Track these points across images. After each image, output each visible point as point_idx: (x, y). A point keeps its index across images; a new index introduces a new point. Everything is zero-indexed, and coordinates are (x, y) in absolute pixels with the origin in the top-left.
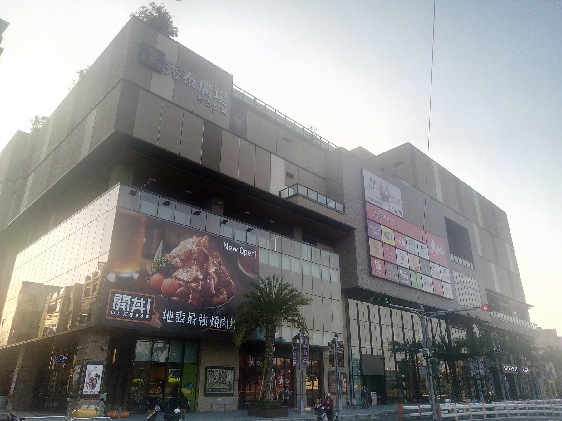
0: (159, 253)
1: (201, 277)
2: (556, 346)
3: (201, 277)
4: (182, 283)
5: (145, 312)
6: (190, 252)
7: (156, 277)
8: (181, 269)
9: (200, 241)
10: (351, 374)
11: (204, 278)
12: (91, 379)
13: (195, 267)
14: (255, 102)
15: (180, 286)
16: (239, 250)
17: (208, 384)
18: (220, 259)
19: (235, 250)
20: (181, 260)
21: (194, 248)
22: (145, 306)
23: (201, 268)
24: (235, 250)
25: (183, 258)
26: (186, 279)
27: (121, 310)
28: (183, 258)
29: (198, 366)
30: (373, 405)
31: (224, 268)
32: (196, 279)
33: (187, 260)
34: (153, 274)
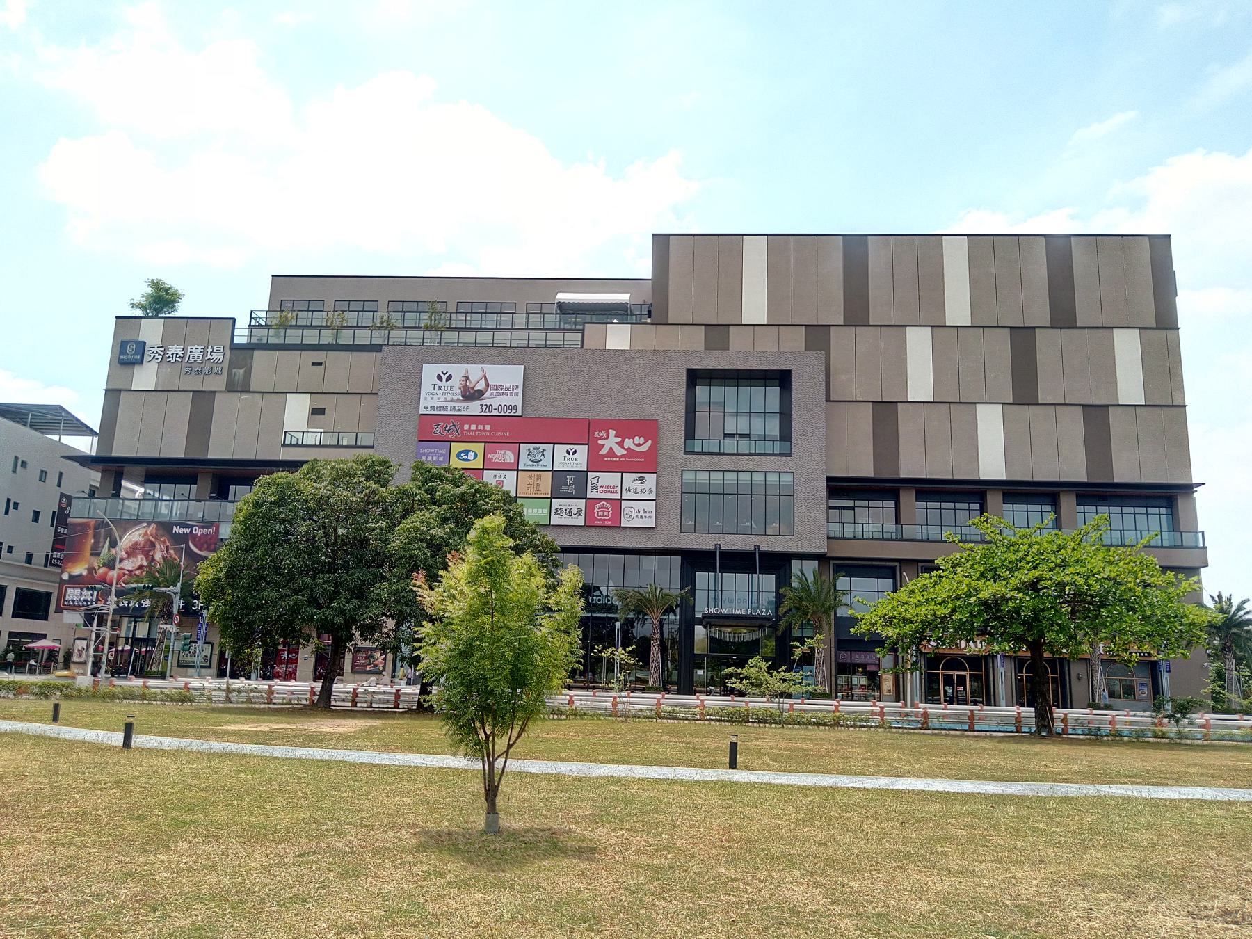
0: (105, 550)
1: (145, 563)
2: (443, 723)
3: (145, 563)
4: (127, 572)
5: (92, 601)
6: (136, 544)
7: (102, 570)
8: (127, 562)
9: (146, 532)
10: (761, 590)
11: (149, 566)
12: (79, 651)
13: (140, 557)
14: (602, 303)
15: (124, 574)
16: (192, 530)
17: (181, 656)
18: (168, 544)
19: (187, 531)
20: (127, 553)
21: (141, 539)
22: (92, 595)
23: (147, 556)
24: (187, 531)
25: (129, 550)
26: (131, 569)
27: (73, 601)
28: (129, 550)
29: (897, 508)
30: (137, 749)
31: (172, 552)
32: (141, 567)
33: (131, 553)
34: (100, 568)
